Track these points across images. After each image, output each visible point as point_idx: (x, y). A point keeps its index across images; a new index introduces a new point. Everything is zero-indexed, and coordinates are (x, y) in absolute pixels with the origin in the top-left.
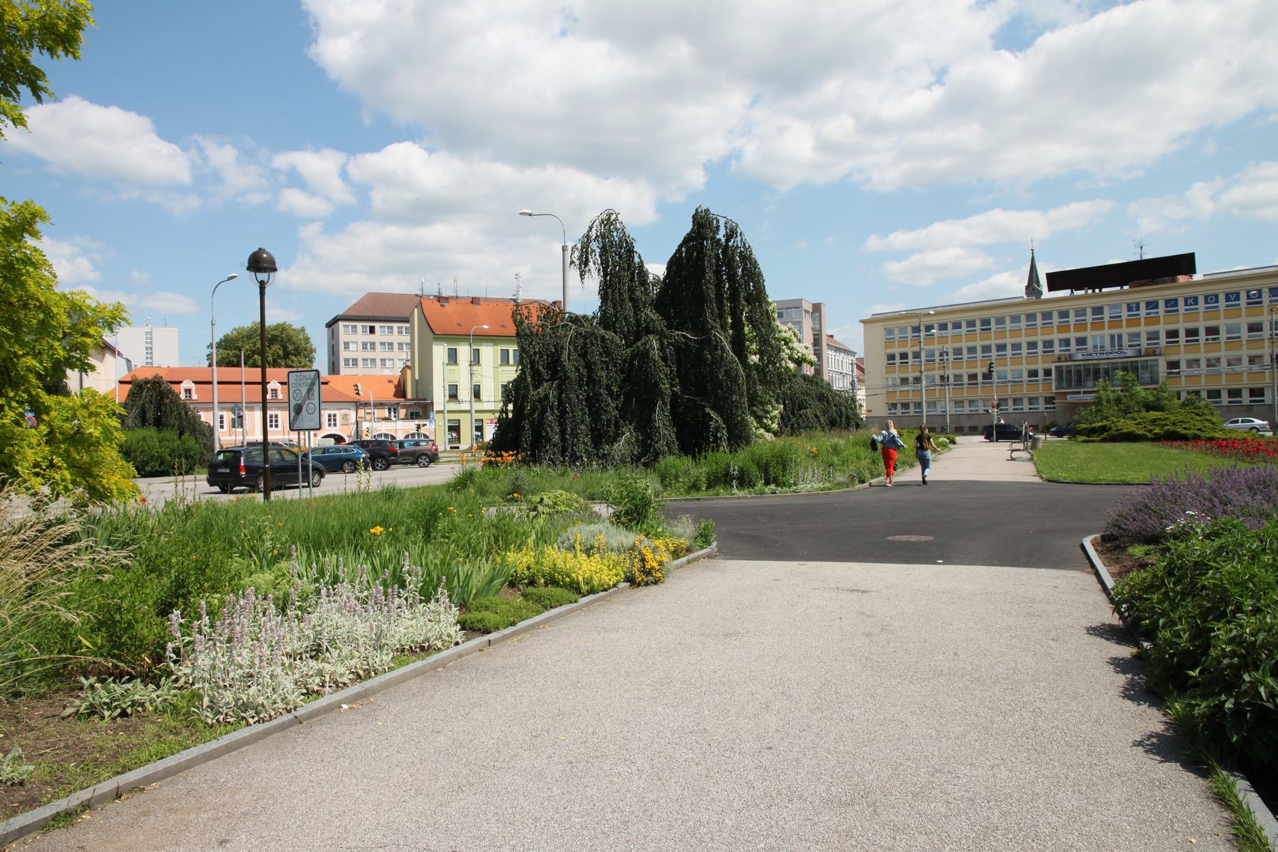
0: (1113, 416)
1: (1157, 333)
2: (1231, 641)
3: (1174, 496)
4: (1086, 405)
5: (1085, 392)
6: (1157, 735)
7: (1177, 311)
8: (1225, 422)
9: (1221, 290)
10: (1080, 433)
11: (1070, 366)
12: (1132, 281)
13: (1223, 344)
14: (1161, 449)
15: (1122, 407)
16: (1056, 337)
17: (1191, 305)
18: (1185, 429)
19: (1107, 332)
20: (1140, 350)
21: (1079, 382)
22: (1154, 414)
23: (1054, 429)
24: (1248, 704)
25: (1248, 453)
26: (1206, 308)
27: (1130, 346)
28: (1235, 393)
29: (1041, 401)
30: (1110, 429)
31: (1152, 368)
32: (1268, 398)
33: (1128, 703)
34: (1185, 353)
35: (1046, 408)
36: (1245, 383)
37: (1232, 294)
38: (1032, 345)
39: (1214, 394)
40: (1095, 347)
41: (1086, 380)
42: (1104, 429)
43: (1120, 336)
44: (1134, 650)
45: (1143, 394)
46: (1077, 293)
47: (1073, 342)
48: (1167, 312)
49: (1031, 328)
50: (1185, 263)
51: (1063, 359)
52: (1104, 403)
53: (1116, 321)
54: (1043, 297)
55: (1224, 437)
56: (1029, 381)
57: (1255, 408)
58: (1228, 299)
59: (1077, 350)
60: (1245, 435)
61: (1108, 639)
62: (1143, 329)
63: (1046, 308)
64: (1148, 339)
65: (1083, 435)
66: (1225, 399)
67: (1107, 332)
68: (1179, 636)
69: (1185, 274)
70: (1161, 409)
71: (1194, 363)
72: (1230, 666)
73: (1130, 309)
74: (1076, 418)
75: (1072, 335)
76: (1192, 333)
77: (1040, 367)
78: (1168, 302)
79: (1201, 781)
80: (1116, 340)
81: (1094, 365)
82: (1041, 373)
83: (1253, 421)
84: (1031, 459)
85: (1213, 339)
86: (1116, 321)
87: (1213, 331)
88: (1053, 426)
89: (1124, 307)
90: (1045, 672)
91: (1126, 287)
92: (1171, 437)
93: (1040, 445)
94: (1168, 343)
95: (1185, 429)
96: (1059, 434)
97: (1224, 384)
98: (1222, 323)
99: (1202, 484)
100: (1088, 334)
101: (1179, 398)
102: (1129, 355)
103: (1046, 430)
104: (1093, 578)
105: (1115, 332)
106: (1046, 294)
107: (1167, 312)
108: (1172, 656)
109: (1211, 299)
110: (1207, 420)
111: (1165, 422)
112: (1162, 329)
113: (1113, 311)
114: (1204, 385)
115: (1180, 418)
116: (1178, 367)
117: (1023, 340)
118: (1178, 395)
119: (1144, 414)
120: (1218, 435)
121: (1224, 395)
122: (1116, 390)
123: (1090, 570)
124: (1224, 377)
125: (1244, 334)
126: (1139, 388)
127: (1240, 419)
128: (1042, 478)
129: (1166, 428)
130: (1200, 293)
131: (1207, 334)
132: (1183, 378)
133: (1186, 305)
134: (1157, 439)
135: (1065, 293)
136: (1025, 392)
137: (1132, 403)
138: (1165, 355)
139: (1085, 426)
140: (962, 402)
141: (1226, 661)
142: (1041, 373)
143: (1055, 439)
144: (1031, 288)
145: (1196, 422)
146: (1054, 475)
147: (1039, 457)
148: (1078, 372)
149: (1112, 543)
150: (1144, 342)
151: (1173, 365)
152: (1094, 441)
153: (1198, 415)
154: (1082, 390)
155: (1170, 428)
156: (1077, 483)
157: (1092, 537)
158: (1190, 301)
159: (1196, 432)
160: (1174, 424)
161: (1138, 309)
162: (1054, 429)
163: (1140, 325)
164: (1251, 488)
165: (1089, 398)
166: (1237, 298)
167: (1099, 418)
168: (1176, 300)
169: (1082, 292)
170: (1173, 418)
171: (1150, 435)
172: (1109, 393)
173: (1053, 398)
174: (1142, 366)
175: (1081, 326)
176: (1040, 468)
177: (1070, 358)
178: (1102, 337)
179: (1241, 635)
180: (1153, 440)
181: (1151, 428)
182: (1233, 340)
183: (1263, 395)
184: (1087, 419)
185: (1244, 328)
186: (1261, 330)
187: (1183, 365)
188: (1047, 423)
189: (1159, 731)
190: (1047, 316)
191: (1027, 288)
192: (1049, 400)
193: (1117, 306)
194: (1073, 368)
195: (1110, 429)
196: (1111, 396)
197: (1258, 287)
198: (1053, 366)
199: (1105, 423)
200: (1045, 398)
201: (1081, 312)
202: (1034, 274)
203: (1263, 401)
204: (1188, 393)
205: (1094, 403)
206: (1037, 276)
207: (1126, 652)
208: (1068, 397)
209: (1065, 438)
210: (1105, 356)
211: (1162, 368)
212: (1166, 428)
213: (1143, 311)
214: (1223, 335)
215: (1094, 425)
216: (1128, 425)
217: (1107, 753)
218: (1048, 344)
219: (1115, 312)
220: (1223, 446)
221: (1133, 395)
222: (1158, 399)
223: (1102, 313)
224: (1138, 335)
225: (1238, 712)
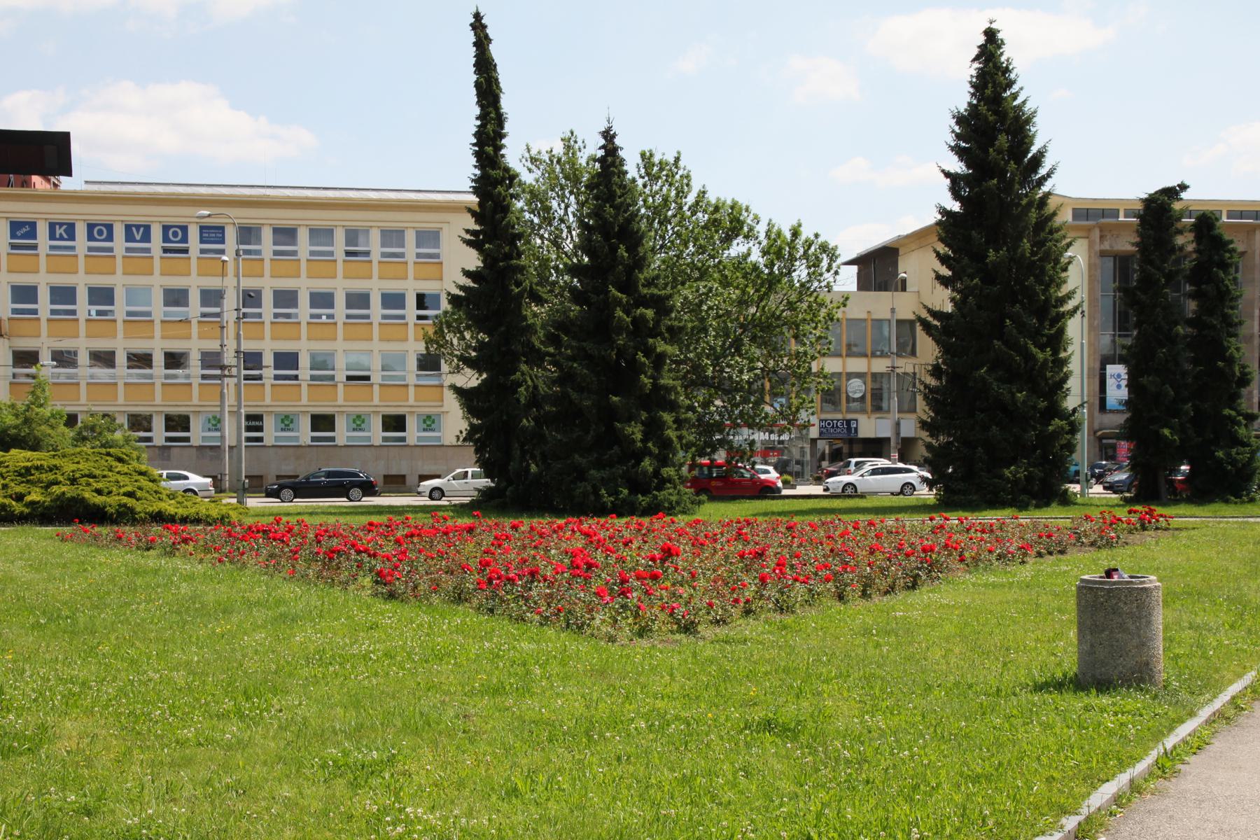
1: (259, 293)
7: (35, 247)
9: (119, 216)
17: (61, 238)
18: (99, 492)
26: (90, 249)
36: (159, 404)
37: (138, 227)
38: (212, 297)
39: (140, 422)
48: (166, 250)
49: (321, 261)
57: (174, 452)
58: (129, 237)
69: (46, 173)
83: (186, 478)
87: (102, 296)
95: (99, 492)
98: (118, 281)
107: (166, 250)
110: (141, 473)
111: (51, 477)
115: (84, 467)
117: (340, 287)
125: (158, 308)
127: (165, 473)
130: (81, 215)
133: (52, 237)
145: (120, 478)
153: (120, 460)
158: (59, 231)
159: (125, 500)
160: (73, 481)
166: (146, 237)
168: (33, 225)
170: (69, 467)
171: (18, 508)
181: (19, 489)
183: (187, 429)
185: (158, 297)
203: (187, 439)
212: (55, 488)
222: (27, 421)
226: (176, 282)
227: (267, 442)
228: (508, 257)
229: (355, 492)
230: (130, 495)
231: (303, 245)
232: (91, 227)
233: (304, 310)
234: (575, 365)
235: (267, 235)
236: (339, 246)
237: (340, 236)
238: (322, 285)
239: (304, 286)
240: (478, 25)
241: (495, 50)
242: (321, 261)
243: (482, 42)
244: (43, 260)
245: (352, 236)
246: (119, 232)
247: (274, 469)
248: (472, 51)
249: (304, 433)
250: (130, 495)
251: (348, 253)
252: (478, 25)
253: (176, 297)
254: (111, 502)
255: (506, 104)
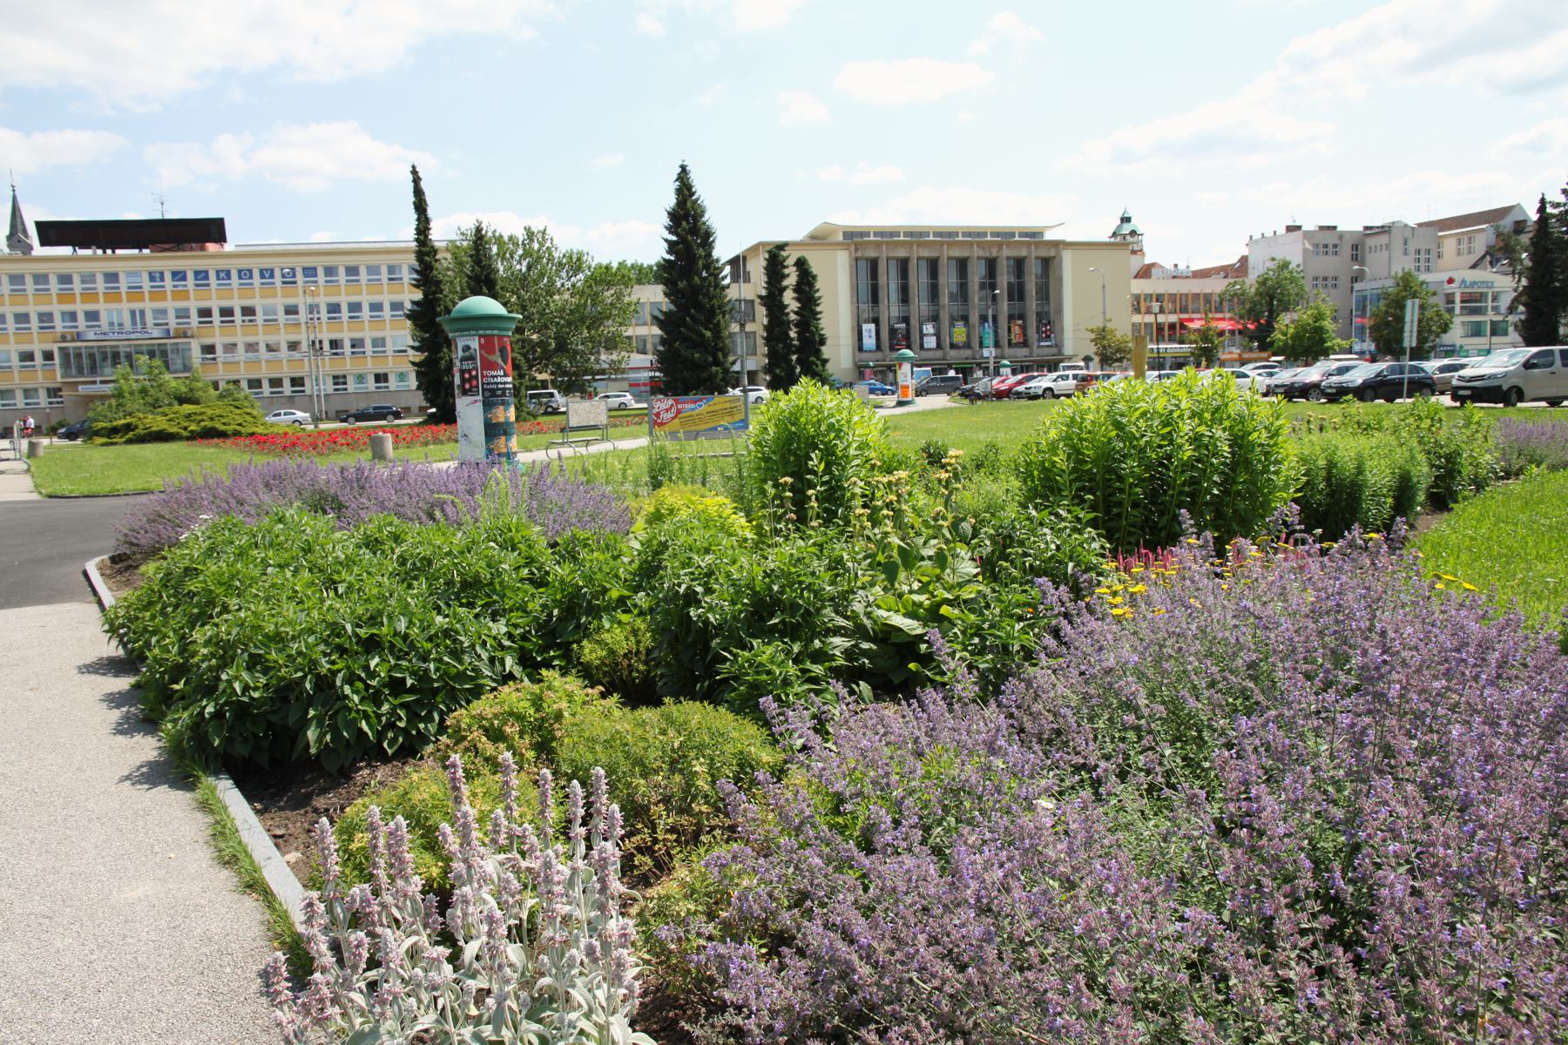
0: (139, 411)
1: (187, 310)
2: (207, 643)
3: (188, 499)
4: (103, 398)
5: (102, 382)
6: (149, 764)
8: (267, 415)
9: (255, 265)
10: (98, 433)
11: (79, 348)
12: (153, 243)
13: (366, 323)
14: (195, 449)
15: (150, 400)
16: (56, 309)
19: (126, 306)
20: (168, 331)
21: (93, 369)
22: (188, 408)
23: (63, 430)
24: (226, 703)
25: (285, 448)
27: (156, 325)
28: (276, 383)
29: (43, 394)
30: (136, 427)
31: (184, 352)
32: (307, 388)
33: (120, 738)
34: (221, 335)
35: (51, 403)
36: (286, 372)
39: (255, 384)
40: (111, 324)
41: (102, 367)
42: (128, 428)
43: (142, 312)
44: (132, 680)
45: (173, 384)
46: (82, 252)
47: (81, 317)
50: (212, 230)
51: (69, 338)
52: (127, 395)
53: (135, 292)
54: (34, 253)
55: (265, 432)
56: (22, 367)
58: (262, 276)
59: (88, 327)
60: (287, 429)
61: (104, 674)
62: (171, 305)
63: (40, 268)
64: (177, 317)
65: (102, 436)
66: (266, 389)
67: (126, 306)
68: (169, 651)
70: (196, 402)
71: (230, 348)
72: (210, 669)
73: (152, 279)
74: (91, 414)
75: (80, 308)
76: (375, 307)
77: (37, 348)
78: (197, 273)
79: (188, 795)
80: (138, 316)
81: (112, 347)
82: (38, 357)
84: (28, 471)
85: (251, 321)
86: (135, 292)
88: (63, 426)
89: (146, 277)
90: (16, 730)
91: (146, 251)
92: (209, 434)
93: (41, 452)
94: (200, 323)
96: (71, 436)
97: (264, 373)
98: (257, 303)
99: (219, 483)
100: (101, 306)
101: (216, 388)
102: (154, 335)
103: (52, 431)
104: (96, 607)
105: (137, 306)
106: (39, 250)
108: (162, 674)
109: (246, 274)
112: (193, 305)
113: (132, 279)
114: (244, 374)
115: (218, 412)
116: (214, 353)
118: (216, 385)
119: (176, 407)
120: (259, 430)
121: (265, 384)
122: (133, 383)
123: (92, 598)
124: (263, 363)
125: (282, 317)
126: (167, 377)
128: (40, 493)
129: (202, 424)
130: (234, 265)
131: (243, 315)
132: (220, 365)
133: (218, 279)
134: (193, 437)
135: (65, 251)
136: (17, 381)
137: (161, 395)
138: (198, 337)
139: (104, 425)
140: (36, 390)
141: (204, 665)
142: (38, 357)
143: (66, 442)
144: (15, 238)
146: (55, 489)
147: (37, 467)
148: (91, 356)
149: (122, 564)
150: (173, 322)
151: (209, 349)
152: (116, 444)
154: (98, 379)
155: (208, 424)
156: (88, 496)
157: (98, 559)
158: (222, 275)
160: (212, 419)
161: (162, 279)
162: (63, 430)
163: (121, 301)
164: (267, 485)
165: (108, 389)
166: (272, 276)
167: (121, 414)
168: (206, 272)
169: (88, 252)
170: (210, 412)
171: (185, 433)
172: (132, 382)
173: (60, 390)
174: (172, 351)
175: (90, 296)
176: (39, 481)
177: (78, 337)
178: (119, 312)
179: (218, 634)
180: (188, 439)
181: (186, 424)
182: (271, 322)
183: (303, 385)
184: (105, 416)
185: (281, 311)
186: (296, 313)
187: (219, 350)
188: (54, 422)
189: (151, 758)
190: (41, 279)
191: (9, 238)
192: (53, 392)
193: (136, 274)
194: (83, 351)
195: (136, 427)
196: (135, 386)
197: (292, 265)
198: (55, 348)
199: (129, 420)
200: (48, 389)
201: (88, 278)
202: (19, 223)
204: (228, 382)
205: (113, 396)
206: (23, 224)
207: (124, 683)
208: (80, 387)
209: (79, 441)
210: (125, 336)
211: (196, 353)
212: (202, 424)
213: (169, 282)
214: (260, 317)
215: (115, 423)
216: (158, 423)
217: (87, 800)
218: (46, 318)
219: (135, 281)
220: (261, 441)
221: (161, 385)
222: (191, 390)
223: (118, 281)
224: (164, 312)
225: (218, 715)
226: (291, 301)
227: (349, 391)
228: (434, 293)
229: (390, 417)
230: (240, 425)
231: (363, 275)
232: (240, 272)
233: (366, 312)
234: (534, 337)
235: (342, 271)
236: (384, 275)
237: (384, 270)
238: (376, 299)
239: (366, 299)
240: (414, 172)
241: (423, 185)
242: (375, 284)
243: (416, 180)
244: (214, 293)
245: (391, 269)
246: (256, 274)
247: (356, 406)
248: (412, 185)
249: (371, 385)
250: (240, 425)
251: (390, 279)
252: (414, 172)
253: (291, 310)
254: (230, 428)
255: (431, 212)
